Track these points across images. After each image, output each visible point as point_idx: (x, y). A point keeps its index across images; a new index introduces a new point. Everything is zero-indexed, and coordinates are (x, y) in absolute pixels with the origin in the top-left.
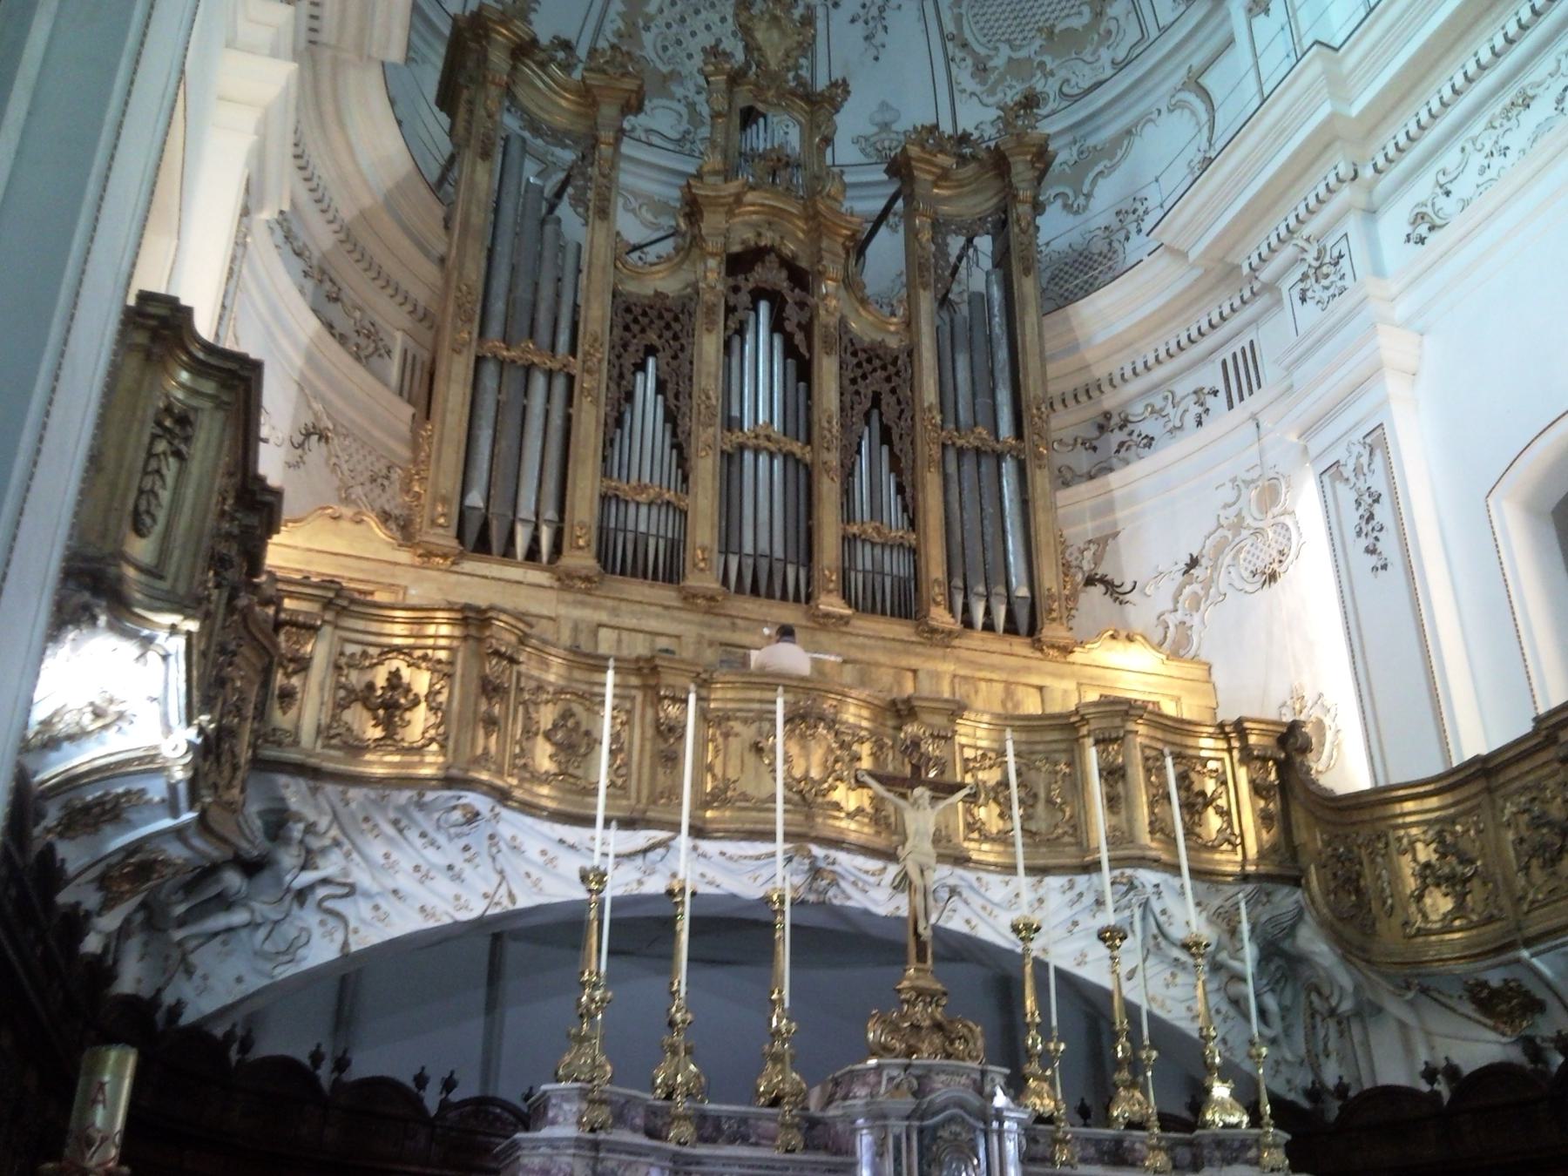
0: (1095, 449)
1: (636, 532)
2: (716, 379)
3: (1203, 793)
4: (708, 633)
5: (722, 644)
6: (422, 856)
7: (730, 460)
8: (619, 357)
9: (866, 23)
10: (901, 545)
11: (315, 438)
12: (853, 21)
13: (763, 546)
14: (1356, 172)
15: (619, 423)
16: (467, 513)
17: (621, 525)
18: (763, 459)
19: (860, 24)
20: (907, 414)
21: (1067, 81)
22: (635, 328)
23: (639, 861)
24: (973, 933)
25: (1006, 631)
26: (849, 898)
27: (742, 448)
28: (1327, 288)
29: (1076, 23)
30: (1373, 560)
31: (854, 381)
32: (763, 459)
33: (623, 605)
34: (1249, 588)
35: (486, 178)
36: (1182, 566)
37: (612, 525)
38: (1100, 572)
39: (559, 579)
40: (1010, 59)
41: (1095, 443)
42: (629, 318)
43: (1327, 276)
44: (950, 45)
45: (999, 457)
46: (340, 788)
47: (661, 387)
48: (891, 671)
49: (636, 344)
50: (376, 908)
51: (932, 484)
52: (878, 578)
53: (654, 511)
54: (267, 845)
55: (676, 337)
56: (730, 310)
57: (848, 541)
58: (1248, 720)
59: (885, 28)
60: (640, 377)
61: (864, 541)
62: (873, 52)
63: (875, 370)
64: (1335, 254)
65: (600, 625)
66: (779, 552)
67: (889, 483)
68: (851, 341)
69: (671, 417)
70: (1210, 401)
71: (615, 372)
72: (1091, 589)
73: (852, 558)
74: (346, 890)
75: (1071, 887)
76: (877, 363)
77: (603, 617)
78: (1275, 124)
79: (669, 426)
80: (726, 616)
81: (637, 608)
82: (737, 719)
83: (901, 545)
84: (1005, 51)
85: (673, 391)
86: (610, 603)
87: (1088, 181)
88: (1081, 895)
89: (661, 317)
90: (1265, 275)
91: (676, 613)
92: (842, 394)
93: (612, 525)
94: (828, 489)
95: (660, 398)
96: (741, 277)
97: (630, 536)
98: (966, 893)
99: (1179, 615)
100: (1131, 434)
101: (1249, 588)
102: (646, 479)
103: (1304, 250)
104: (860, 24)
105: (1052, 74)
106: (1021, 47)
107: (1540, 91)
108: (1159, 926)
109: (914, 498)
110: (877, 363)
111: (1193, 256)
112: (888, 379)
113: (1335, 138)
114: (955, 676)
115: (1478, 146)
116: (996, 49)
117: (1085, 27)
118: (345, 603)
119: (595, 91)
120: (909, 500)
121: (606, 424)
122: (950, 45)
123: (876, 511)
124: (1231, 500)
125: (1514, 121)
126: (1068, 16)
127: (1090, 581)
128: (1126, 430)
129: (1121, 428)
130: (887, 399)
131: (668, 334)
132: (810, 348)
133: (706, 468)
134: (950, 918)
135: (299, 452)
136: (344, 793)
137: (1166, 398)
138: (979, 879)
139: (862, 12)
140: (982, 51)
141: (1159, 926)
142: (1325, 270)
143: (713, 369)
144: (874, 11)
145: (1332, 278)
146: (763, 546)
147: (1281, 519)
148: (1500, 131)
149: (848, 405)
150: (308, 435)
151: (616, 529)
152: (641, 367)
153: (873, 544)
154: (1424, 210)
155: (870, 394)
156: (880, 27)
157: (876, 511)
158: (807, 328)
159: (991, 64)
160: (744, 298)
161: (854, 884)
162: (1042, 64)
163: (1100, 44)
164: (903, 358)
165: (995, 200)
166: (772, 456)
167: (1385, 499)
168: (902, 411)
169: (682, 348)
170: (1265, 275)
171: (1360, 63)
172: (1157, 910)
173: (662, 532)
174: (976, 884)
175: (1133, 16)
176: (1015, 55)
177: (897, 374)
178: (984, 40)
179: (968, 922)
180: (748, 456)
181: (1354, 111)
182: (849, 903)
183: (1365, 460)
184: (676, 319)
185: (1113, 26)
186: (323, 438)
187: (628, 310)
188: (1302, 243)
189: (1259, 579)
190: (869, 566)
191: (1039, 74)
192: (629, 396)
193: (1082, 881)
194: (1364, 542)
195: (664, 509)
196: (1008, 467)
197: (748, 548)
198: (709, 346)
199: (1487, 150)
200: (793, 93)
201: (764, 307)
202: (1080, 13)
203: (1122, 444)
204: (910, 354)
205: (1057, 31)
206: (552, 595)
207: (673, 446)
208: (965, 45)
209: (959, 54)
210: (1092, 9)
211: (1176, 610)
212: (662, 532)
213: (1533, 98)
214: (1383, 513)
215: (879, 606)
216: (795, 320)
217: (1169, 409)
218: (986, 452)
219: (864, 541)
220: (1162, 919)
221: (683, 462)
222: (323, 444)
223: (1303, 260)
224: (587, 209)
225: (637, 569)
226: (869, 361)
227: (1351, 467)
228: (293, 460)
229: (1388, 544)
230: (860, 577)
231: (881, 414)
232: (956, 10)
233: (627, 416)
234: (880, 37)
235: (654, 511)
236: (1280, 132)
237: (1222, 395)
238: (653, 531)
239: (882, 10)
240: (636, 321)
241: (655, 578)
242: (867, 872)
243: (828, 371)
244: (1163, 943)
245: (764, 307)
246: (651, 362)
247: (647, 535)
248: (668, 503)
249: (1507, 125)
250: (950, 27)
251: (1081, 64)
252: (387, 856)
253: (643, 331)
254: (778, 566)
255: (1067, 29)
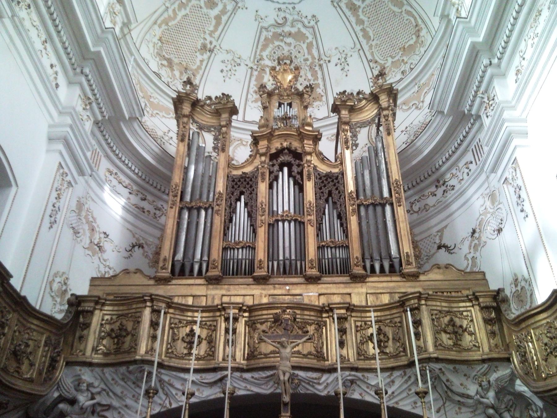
0: (435, 195)
1: (340, 258)
2: (266, 198)
3: (461, 327)
4: (264, 292)
5: (270, 295)
6: (135, 391)
7: (272, 226)
8: (230, 198)
9: (341, 64)
10: (342, 246)
11: (137, 247)
12: (336, 65)
13: (287, 255)
14: (490, 62)
15: (231, 220)
16: (176, 263)
17: (232, 257)
18: (286, 224)
19: (339, 65)
20: (343, 197)
21: (412, 63)
22: (235, 187)
23: (219, 384)
24: (363, 399)
25: (390, 272)
26: (308, 389)
27: (277, 221)
28: (492, 110)
29: (412, 42)
30: (523, 214)
31: (320, 189)
32: (286, 224)
33: (232, 287)
34: (494, 237)
35: (183, 147)
36: (470, 234)
37: (229, 257)
38: (443, 243)
39: (207, 281)
40: (392, 62)
41: (435, 193)
42: (234, 183)
43: (492, 105)
44: (371, 64)
45: (383, 206)
46: (101, 369)
47: (246, 205)
48: (388, 295)
49: (237, 193)
50: (119, 413)
51: (353, 221)
52: (334, 260)
53: (244, 250)
54: (74, 392)
55: (251, 187)
56: (271, 173)
57: (320, 248)
58: (477, 292)
59: (348, 64)
60: (238, 203)
61: (327, 247)
62: (345, 74)
63: (329, 183)
64: (493, 95)
65: (223, 295)
66: (293, 257)
67: (337, 223)
68: (319, 174)
69: (250, 215)
70: (471, 166)
71: (229, 204)
72: (440, 250)
73: (323, 254)
74: (107, 408)
75: (405, 374)
76: (329, 180)
77: (224, 292)
78: (455, 53)
79: (249, 218)
80: (271, 284)
81: (237, 287)
82: (258, 323)
83: (342, 246)
84: (390, 60)
85: (250, 206)
86: (226, 287)
87: (422, 97)
88: (410, 377)
89: (245, 181)
90: (473, 112)
91: (252, 286)
92: (316, 194)
93: (229, 257)
94: (311, 231)
95: (246, 209)
96: (275, 161)
97: (235, 261)
98: (358, 383)
99: (472, 255)
100: (447, 186)
101: (494, 237)
102: (241, 239)
103: (483, 98)
104: (339, 65)
105: (407, 63)
106: (395, 57)
107: (543, 7)
108: (447, 387)
109: (347, 227)
110: (329, 180)
111: (446, 112)
112: (335, 185)
113: (478, 52)
114: (367, 294)
115: (529, 37)
116: (387, 60)
117: (415, 43)
118: (103, 301)
119: (220, 111)
120: (345, 228)
121: (225, 221)
122: (371, 64)
123: (332, 234)
124: (482, 203)
125: (537, 22)
126: (409, 41)
127: (439, 247)
128: (445, 185)
129: (443, 185)
130: (335, 192)
131: (248, 186)
132: (302, 180)
133: (262, 232)
134: (352, 393)
135: (130, 253)
136: (103, 370)
137: (456, 169)
138: (363, 376)
139: (339, 61)
140: (383, 62)
141: (447, 387)
142: (490, 103)
143: (264, 195)
144: (343, 60)
145: (493, 105)
146: (287, 255)
147: (499, 206)
148: (534, 28)
149: (318, 197)
150: (133, 246)
151: (230, 259)
152: (239, 199)
153: (331, 248)
154: (518, 68)
155: (327, 192)
156: (346, 64)
157: (332, 234)
158: (301, 173)
159: (386, 66)
160: (276, 168)
161: (308, 384)
162: (403, 60)
163: (420, 47)
164: (340, 176)
165: (376, 111)
166: (290, 222)
167: (523, 188)
168: (341, 196)
169: (253, 190)
170: (473, 112)
171: (476, 20)
172: (444, 380)
173: (247, 257)
174: (362, 378)
175: (429, 33)
176: (394, 60)
177: (338, 182)
178: (382, 58)
179: (361, 394)
180: (280, 224)
181: (481, 39)
182: (309, 392)
183: (514, 174)
184: (251, 180)
185: (423, 39)
186: (141, 246)
187: (233, 181)
188: (481, 95)
189: (496, 232)
190: (330, 256)
191: (402, 64)
192: (234, 211)
193: (408, 371)
194: (520, 208)
195: (248, 249)
196: (388, 208)
197: (281, 258)
198: (263, 187)
199: (532, 37)
200: (293, 94)
201: (286, 169)
202: (412, 38)
203: (444, 191)
204: (343, 174)
205: (406, 47)
206: (204, 288)
207: (251, 225)
208: (376, 62)
209: (375, 65)
210: (416, 35)
211: (470, 253)
212: (247, 257)
213: (541, 11)
214: (523, 194)
215: (335, 270)
216: (296, 171)
217: (458, 174)
218: (377, 205)
219: (327, 247)
220: (448, 384)
221: (255, 231)
222: (140, 249)
223: (484, 102)
224: (219, 150)
225: (237, 273)
226: (326, 180)
227: (511, 178)
228: (126, 256)
229: (527, 207)
230: (327, 261)
231: (332, 198)
232: (371, 51)
233: (234, 218)
234: (347, 68)
235: (244, 250)
236: (457, 56)
237: (474, 162)
238: (244, 257)
239: (345, 58)
240: (236, 184)
241: (329, 273)
242: (313, 378)
243: (309, 187)
244: (450, 393)
245: (286, 169)
246: (243, 197)
247: (242, 259)
248: (249, 246)
249: (536, 25)
250: (370, 57)
251: (415, 56)
252: (122, 393)
253: (239, 187)
254: (293, 262)
255: (410, 45)
